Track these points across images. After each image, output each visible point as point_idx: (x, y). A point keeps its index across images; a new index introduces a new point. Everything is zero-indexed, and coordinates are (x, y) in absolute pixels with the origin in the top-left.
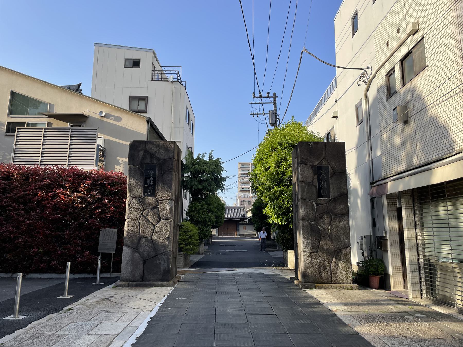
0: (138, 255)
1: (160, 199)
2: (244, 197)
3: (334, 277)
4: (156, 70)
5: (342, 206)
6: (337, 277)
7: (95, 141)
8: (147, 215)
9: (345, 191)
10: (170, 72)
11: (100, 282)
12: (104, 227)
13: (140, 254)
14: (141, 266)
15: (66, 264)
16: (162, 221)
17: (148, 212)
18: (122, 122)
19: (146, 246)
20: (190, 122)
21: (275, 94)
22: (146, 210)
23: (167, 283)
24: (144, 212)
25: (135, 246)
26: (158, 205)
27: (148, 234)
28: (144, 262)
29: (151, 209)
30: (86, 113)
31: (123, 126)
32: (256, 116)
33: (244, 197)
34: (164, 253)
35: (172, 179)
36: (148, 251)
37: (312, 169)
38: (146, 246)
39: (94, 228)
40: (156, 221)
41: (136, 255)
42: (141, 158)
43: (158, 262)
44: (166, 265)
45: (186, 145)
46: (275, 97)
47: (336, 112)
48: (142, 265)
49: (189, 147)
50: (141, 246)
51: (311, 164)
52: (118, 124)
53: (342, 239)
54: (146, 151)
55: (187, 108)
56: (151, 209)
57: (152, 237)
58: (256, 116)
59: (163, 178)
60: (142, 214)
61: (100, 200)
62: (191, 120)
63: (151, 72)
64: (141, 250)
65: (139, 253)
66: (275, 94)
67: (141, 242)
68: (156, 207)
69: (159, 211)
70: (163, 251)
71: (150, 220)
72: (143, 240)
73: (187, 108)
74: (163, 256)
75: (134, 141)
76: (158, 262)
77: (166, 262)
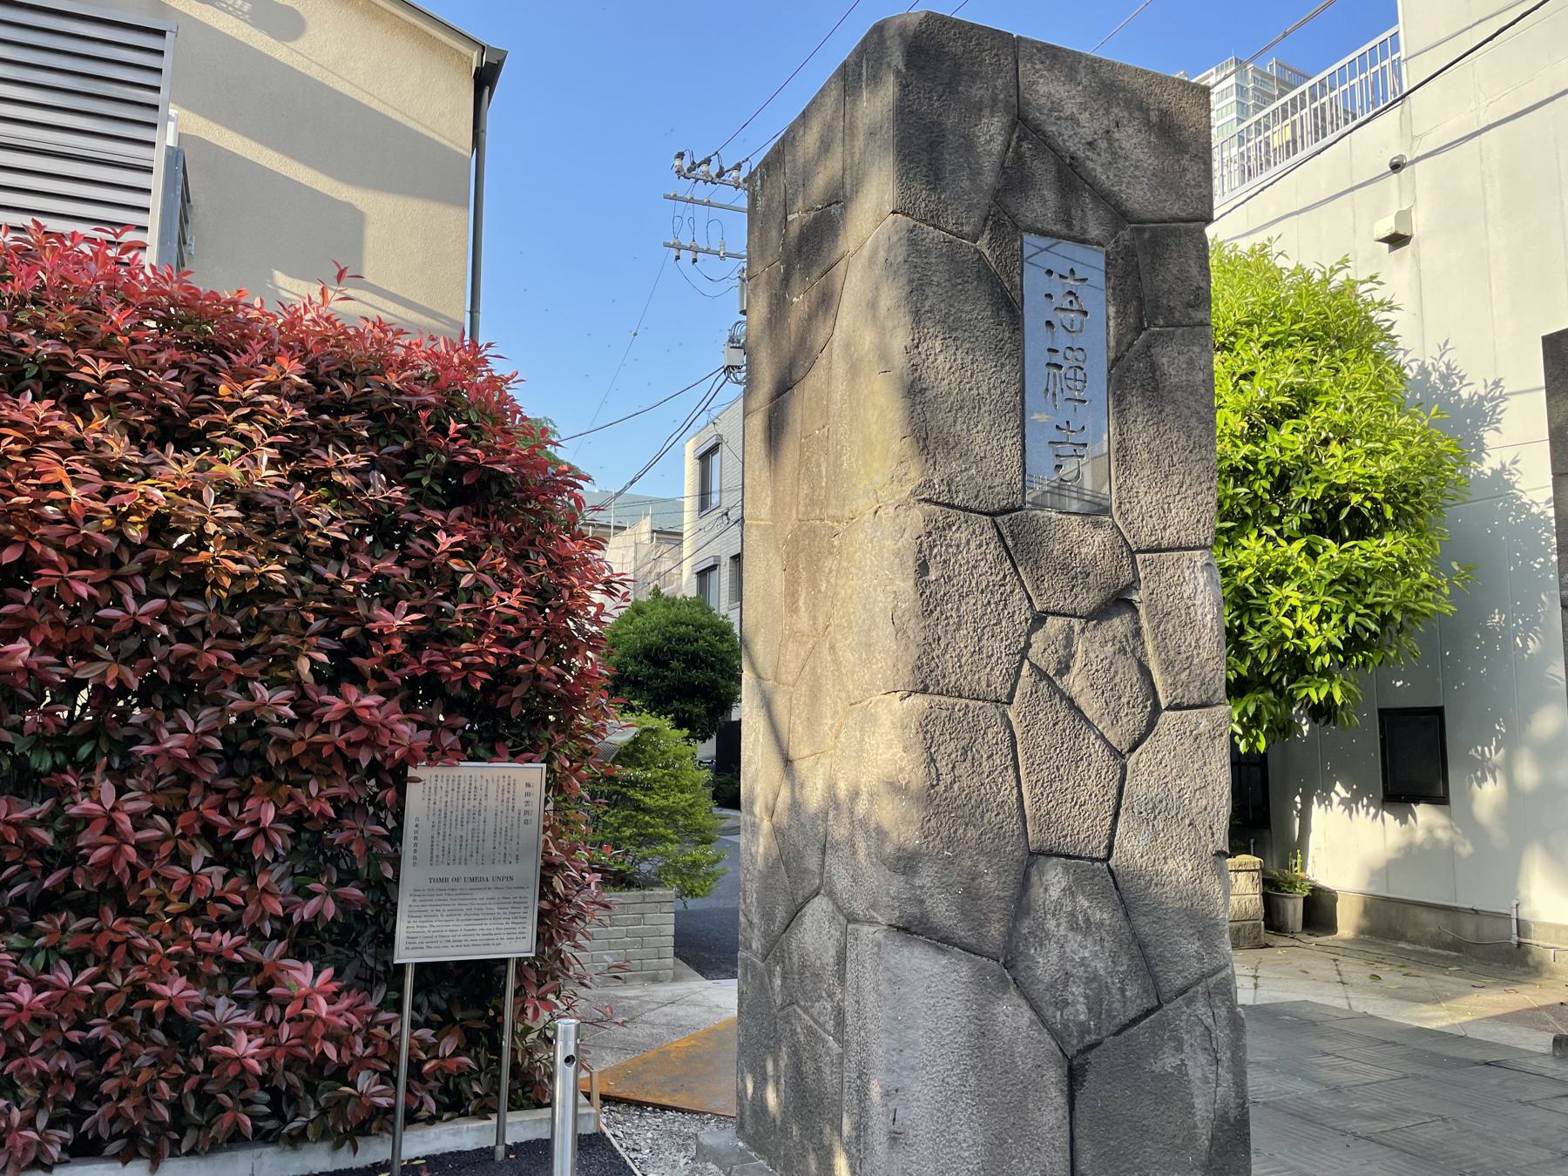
0: (1027, 1015)
1: (1146, 540)
7: (147, 116)
8: (1064, 668)
12: (435, 754)
13: (1034, 1008)
14: (1050, 1112)
16: (1168, 717)
17: (1069, 642)
18: (302, 44)
19: (1074, 927)
22: (1054, 624)
24: (1038, 639)
25: (995, 930)
26: (1133, 585)
27: (1082, 824)
28: (1074, 1077)
29: (1089, 617)
31: (314, 72)
32: (687, 256)
36: (1092, 979)
38: (1074, 927)
39: (364, 758)
40: (1132, 721)
42: (988, 179)
43: (1169, 1061)
44: (1225, 1089)
47: (1404, 216)
48: (1056, 1097)
50: (1041, 937)
52: (280, 52)
56: (1089, 617)
57: (1110, 848)
58: (687, 256)
59: (1153, 367)
60: (1024, 653)
61: (385, 528)
64: (1044, 964)
67: (1036, 891)
68: (1118, 602)
69: (1137, 633)
70: (1194, 968)
71: (1091, 706)
72: (1053, 882)
74: (1201, 1009)
75: (930, 16)
76: (1169, 1061)
77: (1225, 1056)
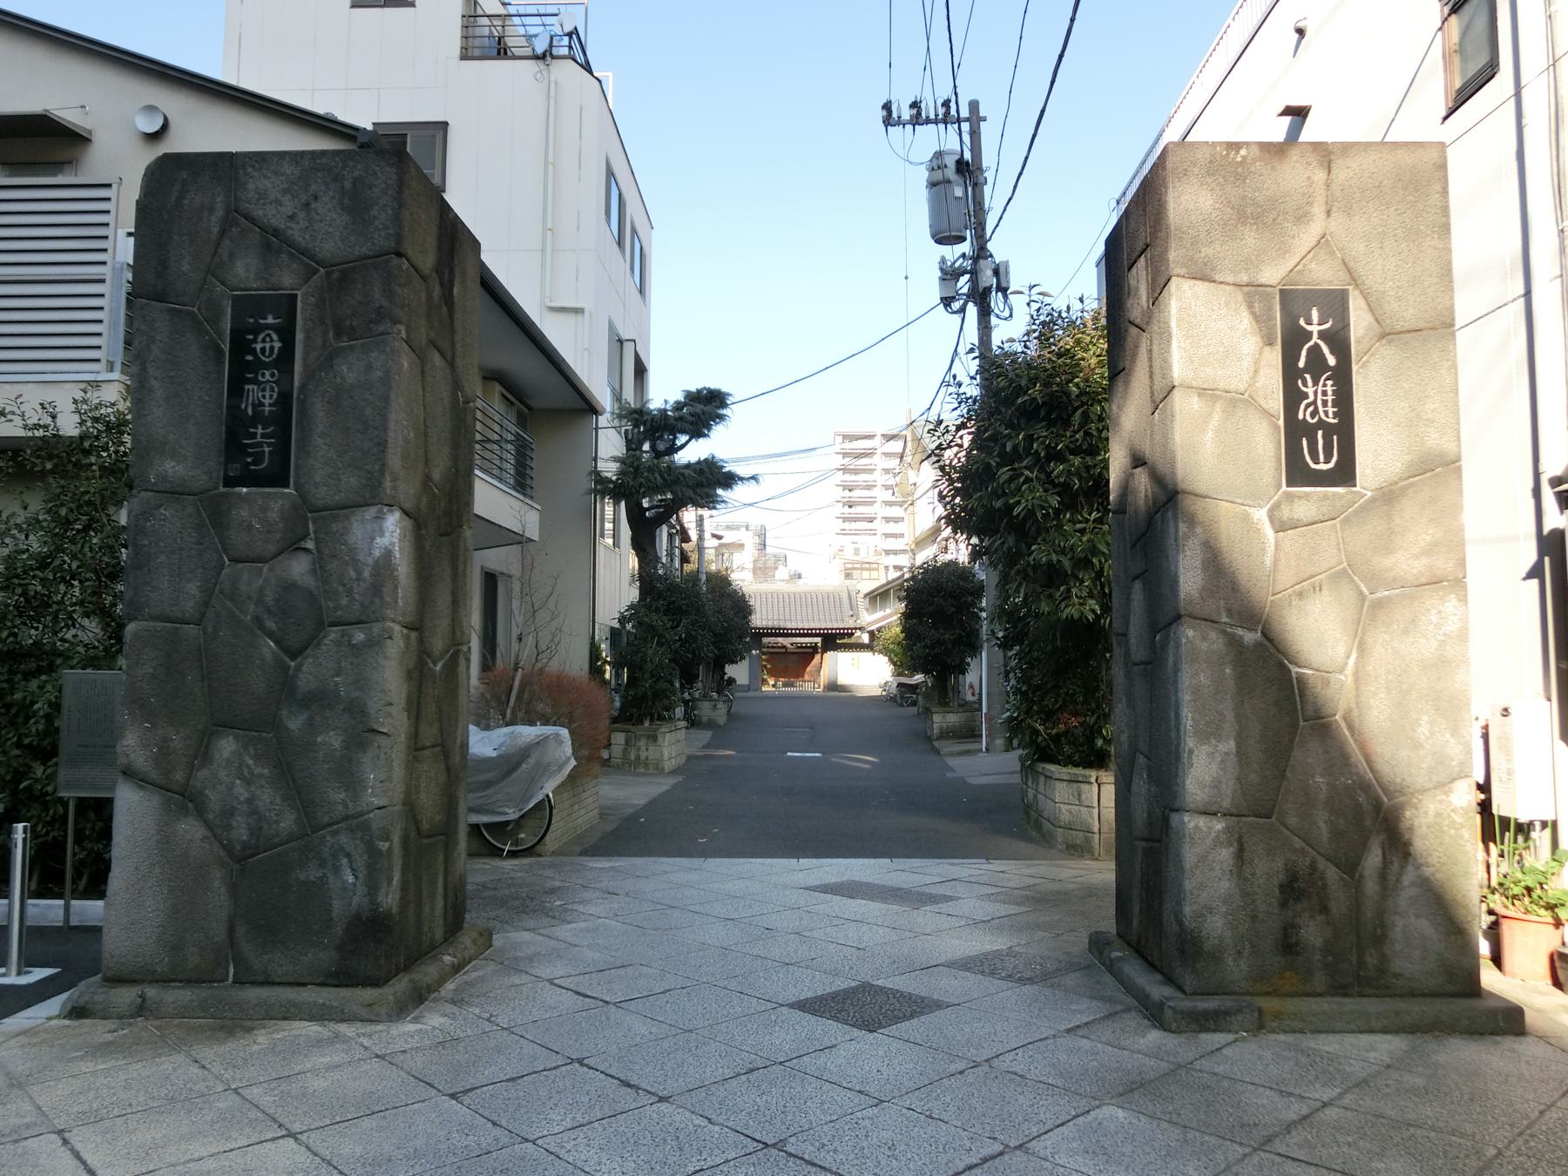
2: (857, 552)
3: (1371, 959)
4: (480, 12)
5: (1425, 534)
6: (1384, 958)
9: (1449, 446)
10: (537, 20)
11: (27, 962)
15: (10, 832)
20: (628, 237)
21: (974, 106)
23: (369, 994)
30: (70, 116)
33: (857, 552)
34: (347, 818)
35: (386, 381)
37: (1250, 306)
41: (190, 830)
45: (612, 327)
46: (975, 118)
49: (625, 336)
51: (1244, 278)
53: (1423, 729)
54: (236, 216)
55: (610, 173)
62: (634, 231)
63: (458, 22)
65: (200, 812)
66: (974, 106)
73: (610, 173)
